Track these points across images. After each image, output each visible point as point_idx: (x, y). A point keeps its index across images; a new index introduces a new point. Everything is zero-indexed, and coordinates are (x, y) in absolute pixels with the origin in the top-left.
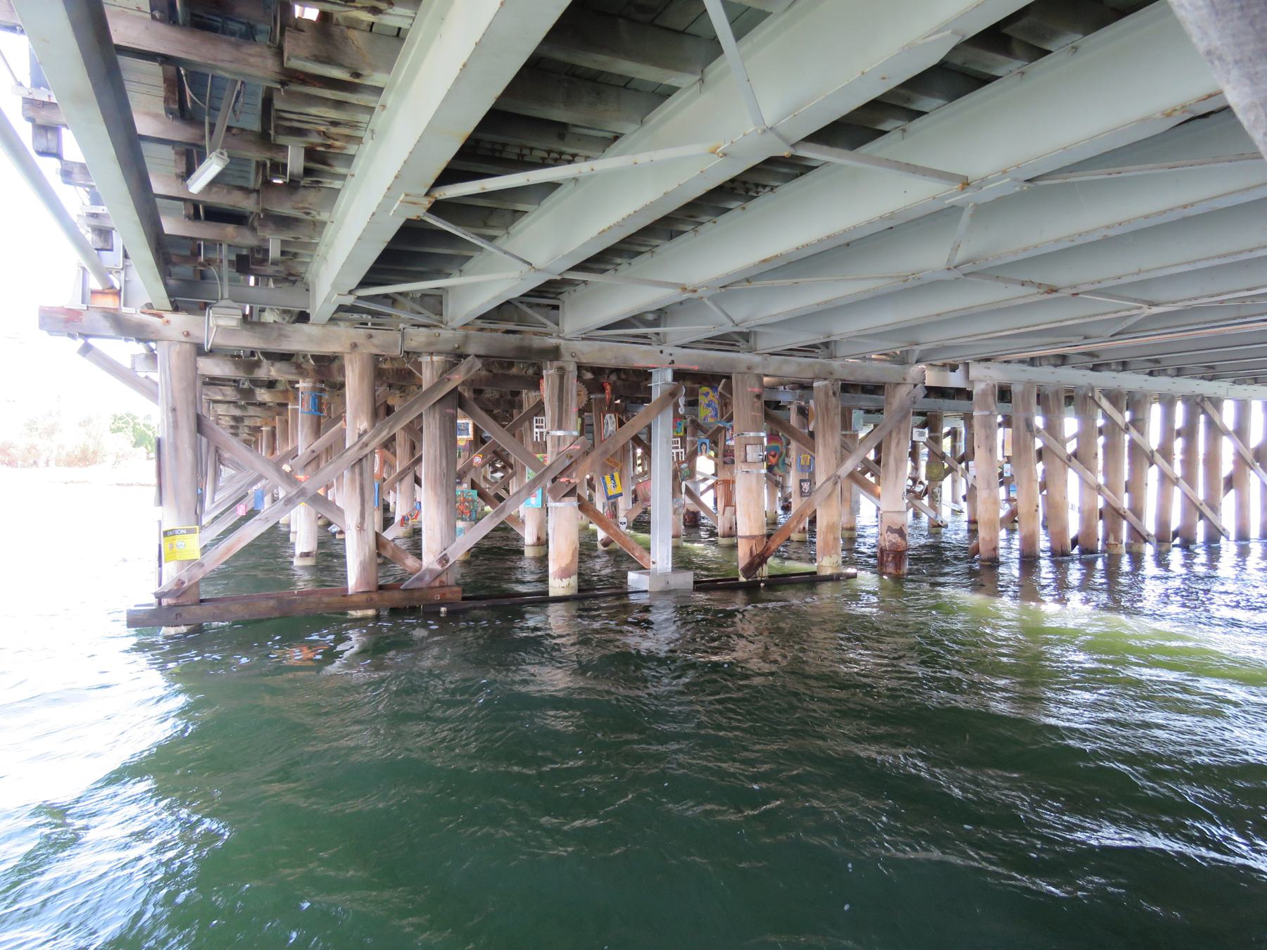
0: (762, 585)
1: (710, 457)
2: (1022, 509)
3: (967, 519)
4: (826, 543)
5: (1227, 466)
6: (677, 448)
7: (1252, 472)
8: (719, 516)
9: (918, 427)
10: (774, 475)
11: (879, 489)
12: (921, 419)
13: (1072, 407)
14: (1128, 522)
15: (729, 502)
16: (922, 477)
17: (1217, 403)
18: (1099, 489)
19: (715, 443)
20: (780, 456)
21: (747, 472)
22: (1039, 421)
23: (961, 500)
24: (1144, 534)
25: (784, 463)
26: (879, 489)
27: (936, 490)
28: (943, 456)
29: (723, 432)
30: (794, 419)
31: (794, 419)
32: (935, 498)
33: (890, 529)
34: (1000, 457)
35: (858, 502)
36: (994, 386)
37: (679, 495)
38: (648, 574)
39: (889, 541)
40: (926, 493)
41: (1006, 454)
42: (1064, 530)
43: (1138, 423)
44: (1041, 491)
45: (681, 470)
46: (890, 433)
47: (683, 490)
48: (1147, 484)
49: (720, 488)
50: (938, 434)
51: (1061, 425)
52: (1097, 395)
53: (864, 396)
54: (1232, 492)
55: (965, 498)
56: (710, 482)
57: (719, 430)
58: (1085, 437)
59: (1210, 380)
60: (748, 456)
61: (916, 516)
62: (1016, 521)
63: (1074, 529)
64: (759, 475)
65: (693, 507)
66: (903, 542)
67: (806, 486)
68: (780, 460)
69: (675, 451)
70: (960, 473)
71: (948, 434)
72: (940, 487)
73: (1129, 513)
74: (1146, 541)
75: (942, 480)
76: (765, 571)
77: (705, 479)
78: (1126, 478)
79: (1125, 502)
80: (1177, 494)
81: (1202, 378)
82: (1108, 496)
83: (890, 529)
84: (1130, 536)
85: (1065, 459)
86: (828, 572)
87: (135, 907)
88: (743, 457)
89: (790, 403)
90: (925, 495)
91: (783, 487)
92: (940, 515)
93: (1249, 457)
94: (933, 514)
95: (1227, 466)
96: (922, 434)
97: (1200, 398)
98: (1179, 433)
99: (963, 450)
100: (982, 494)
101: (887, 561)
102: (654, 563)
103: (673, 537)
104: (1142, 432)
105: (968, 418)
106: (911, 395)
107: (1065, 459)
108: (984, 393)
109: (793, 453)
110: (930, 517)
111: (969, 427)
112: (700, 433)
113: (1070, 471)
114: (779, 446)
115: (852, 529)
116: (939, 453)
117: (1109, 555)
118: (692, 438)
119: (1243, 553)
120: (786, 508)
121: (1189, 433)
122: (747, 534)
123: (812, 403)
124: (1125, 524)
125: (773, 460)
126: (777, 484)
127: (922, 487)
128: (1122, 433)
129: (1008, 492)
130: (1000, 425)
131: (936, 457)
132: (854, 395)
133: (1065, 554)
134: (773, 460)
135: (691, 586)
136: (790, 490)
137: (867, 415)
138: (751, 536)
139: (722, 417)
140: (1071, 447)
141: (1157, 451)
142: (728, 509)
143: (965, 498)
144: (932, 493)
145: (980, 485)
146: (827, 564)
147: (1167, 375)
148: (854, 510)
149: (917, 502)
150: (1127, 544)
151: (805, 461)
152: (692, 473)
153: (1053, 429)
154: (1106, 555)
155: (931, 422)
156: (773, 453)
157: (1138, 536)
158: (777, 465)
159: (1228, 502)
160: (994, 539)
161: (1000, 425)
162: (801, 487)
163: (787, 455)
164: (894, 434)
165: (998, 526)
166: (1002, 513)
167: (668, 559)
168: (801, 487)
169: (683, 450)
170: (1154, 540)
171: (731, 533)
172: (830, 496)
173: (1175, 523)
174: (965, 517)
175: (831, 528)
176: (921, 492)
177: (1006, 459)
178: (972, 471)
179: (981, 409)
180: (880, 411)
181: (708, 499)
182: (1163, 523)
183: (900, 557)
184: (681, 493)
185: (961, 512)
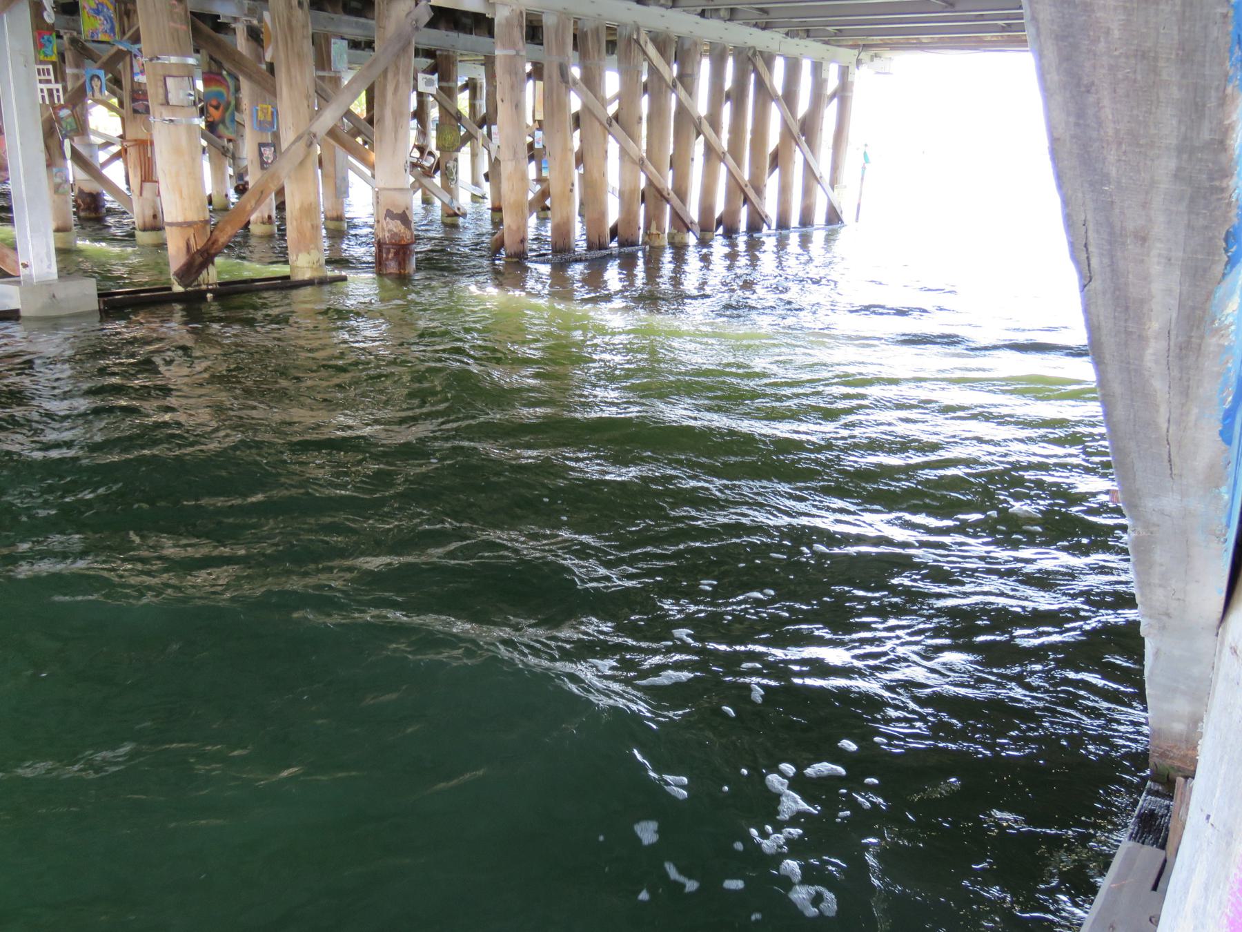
0: (209, 296)
1: (111, 108)
2: (554, 189)
3: (490, 206)
4: (300, 232)
5: (773, 139)
6: (48, 81)
7: (797, 149)
8: (135, 198)
9: (425, 71)
10: (220, 137)
11: (373, 156)
12: (426, 62)
13: (615, 57)
14: (705, 136)
15: (148, 176)
16: (433, 144)
17: (769, 60)
18: (641, 164)
19: (117, 82)
20: (227, 108)
21: (171, 121)
22: (576, 72)
23: (483, 179)
24: (687, 221)
25: (233, 120)
26: (373, 156)
27: (451, 165)
28: (458, 117)
29: (128, 59)
30: (241, 43)
31: (241, 43)
32: (449, 176)
33: (390, 214)
34: (530, 121)
35: (345, 179)
36: (521, 13)
37: (59, 161)
38: (18, 283)
39: (389, 231)
40: (438, 167)
41: (538, 117)
42: (603, 215)
43: (686, 80)
44: (577, 167)
45: (59, 120)
46: (385, 72)
47: (68, 153)
48: (693, 159)
49: (132, 153)
50: (451, 84)
51: (601, 77)
52: (644, 38)
53: (346, 18)
54: (777, 171)
55: (487, 176)
56: (115, 149)
57: (120, 56)
58: (627, 97)
59: (764, 29)
60: (170, 96)
61: (426, 201)
62: (548, 209)
63: (613, 215)
64: (190, 127)
65: (91, 186)
66: (408, 232)
67: (268, 153)
68: (228, 114)
69: (45, 87)
70: (480, 142)
71: (465, 87)
72: (456, 160)
73: (673, 196)
74: (689, 230)
75: (458, 150)
76: (212, 275)
77: (108, 144)
78: (671, 152)
79: (668, 182)
80: (723, 171)
81: (756, 25)
82: (651, 172)
83: (390, 214)
84: (672, 223)
85: (605, 122)
86: (307, 275)
87: (1228, 395)
88: (161, 97)
89: (235, 19)
90: (435, 172)
91: (234, 157)
92: (457, 200)
93: (796, 129)
94: (447, 199)
95: (773, 139)
96: (429, 83)
97: (752, 51)
98: (728, 97)
99: (484, 111)
100: (507, 168)
101: (387, 259)
102: (25, 266)
103: (58, 230)
104: (690, 91)
105: (489, 62)
106: (412, 16)
107: (605, 122)
108: (508, 22)
109: (246, 103)
110: (443, 203)
111: (491, 76)
112: (88, 62)
113: (610, 138)
114: (223, 90)
115: (339, 218)
116: (453, 112)
117: (651, 247)
118: (75, 71)
119: (782, 244)
120: (241, 190)
121: (737, 97)
122: (180, 220)
123: (267, 16)
124: (668, 207)
125: (216, 114)
126: (224, 152)
127: (432, 160)
128: (669, 91)
129: (539, 170)
130: (529, 76)
131: (450, 117)
132: (333, 16)
133: (602, 246)
134: (216, 114)
135: (93, 304)
136: (245, 163)
137: (353, 51)
138: (185, 223)
139: (123, 33)
140: (612, 109)
141: (705, 117)
142: (147, 185)
143: (487, 176)
144: (445, 169)
145: (505, 157)
146: (304, 264)
147: (719, 18)
148: (340, 191)
149: (425, 181)
150: (669, 234)
151: (265, 114)
152: (81, 128)
153: (591, 82)
154: (648, 247)
155: (441, 65)
156: (214, 103)
157: (681, 223)
158: (223, 121)
159: (772, 183)
160: (523, 227)
161: (529, 76)
162: (261, 155)
163: (238, 108)
164: (390, 75)
165: (527, 211)
166: (531, 196)
167: (50, 260)
168: (261, 155)
169: (60, 86)
170: (697, 229)
171: (155, 225)
172: (302, 163)
173: (719, 208)
174: (488, 203)
175: (309, 210)
176: (430, 168)
177: (537, 125)
178: (496, 140)
179: (504, 46)
180: (369, 45)
181: (115, 173)
182: (706, 209)
183: (405, 253)
184: (64, 158)
185: (483, 197)
